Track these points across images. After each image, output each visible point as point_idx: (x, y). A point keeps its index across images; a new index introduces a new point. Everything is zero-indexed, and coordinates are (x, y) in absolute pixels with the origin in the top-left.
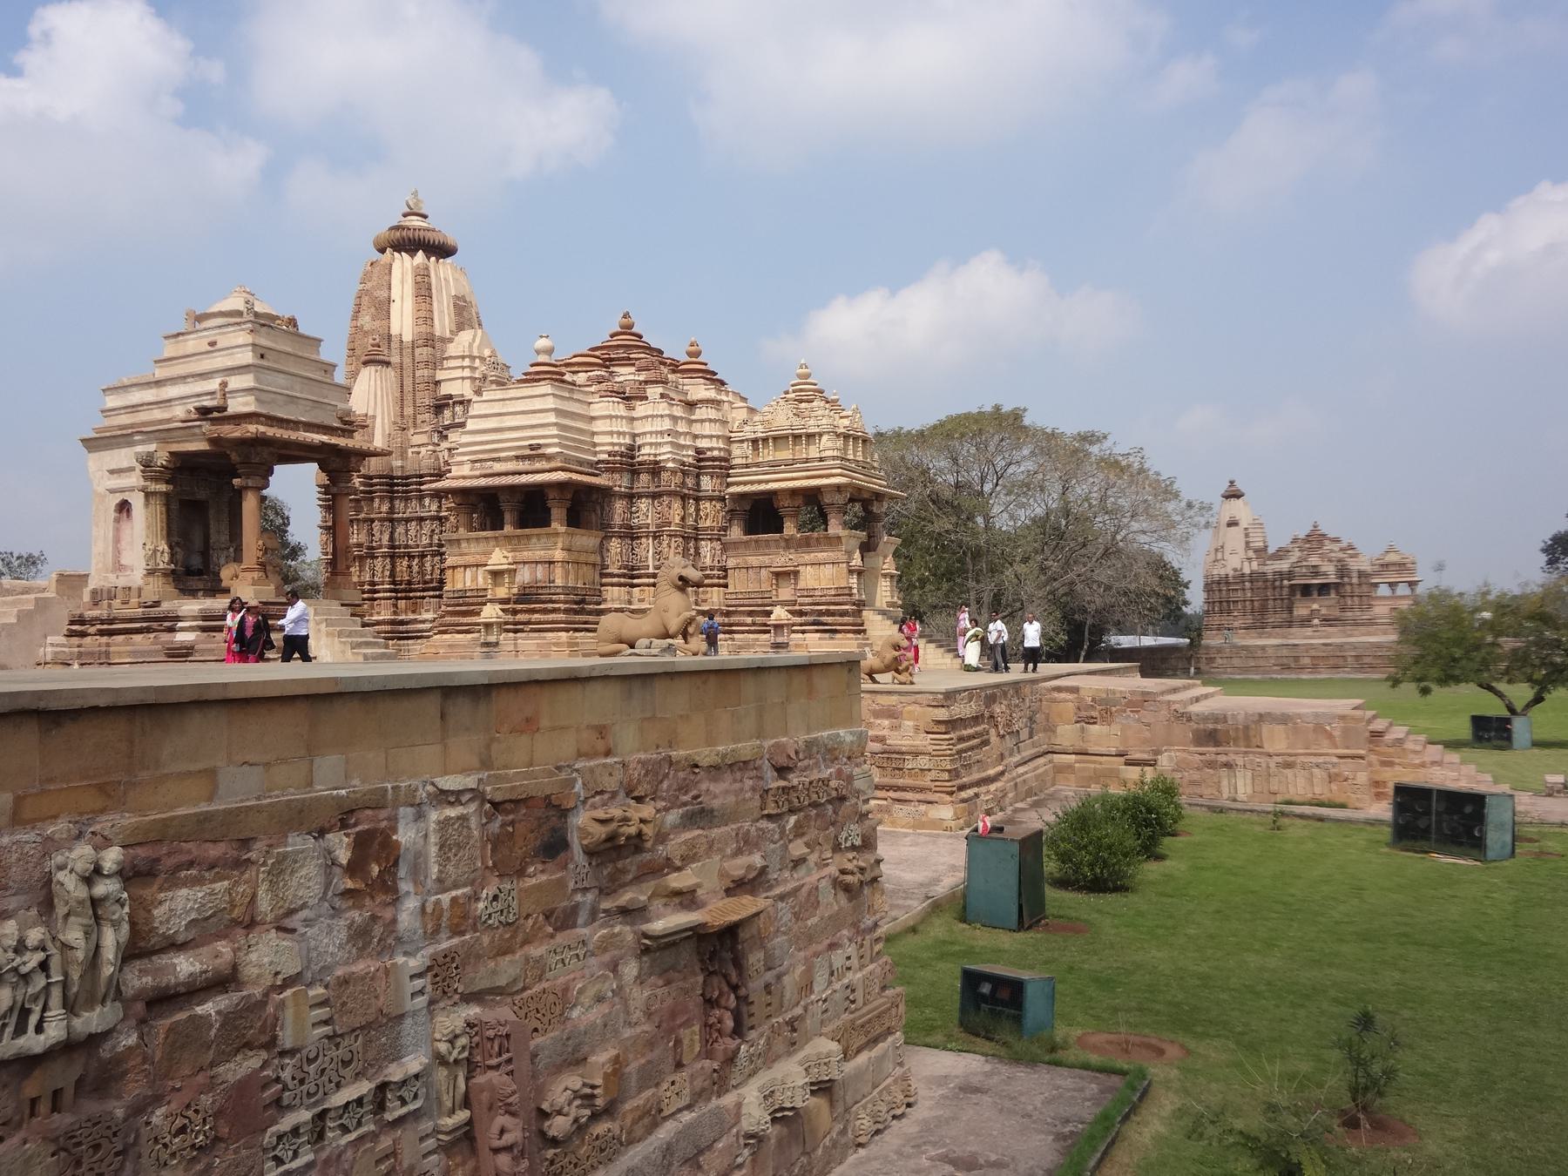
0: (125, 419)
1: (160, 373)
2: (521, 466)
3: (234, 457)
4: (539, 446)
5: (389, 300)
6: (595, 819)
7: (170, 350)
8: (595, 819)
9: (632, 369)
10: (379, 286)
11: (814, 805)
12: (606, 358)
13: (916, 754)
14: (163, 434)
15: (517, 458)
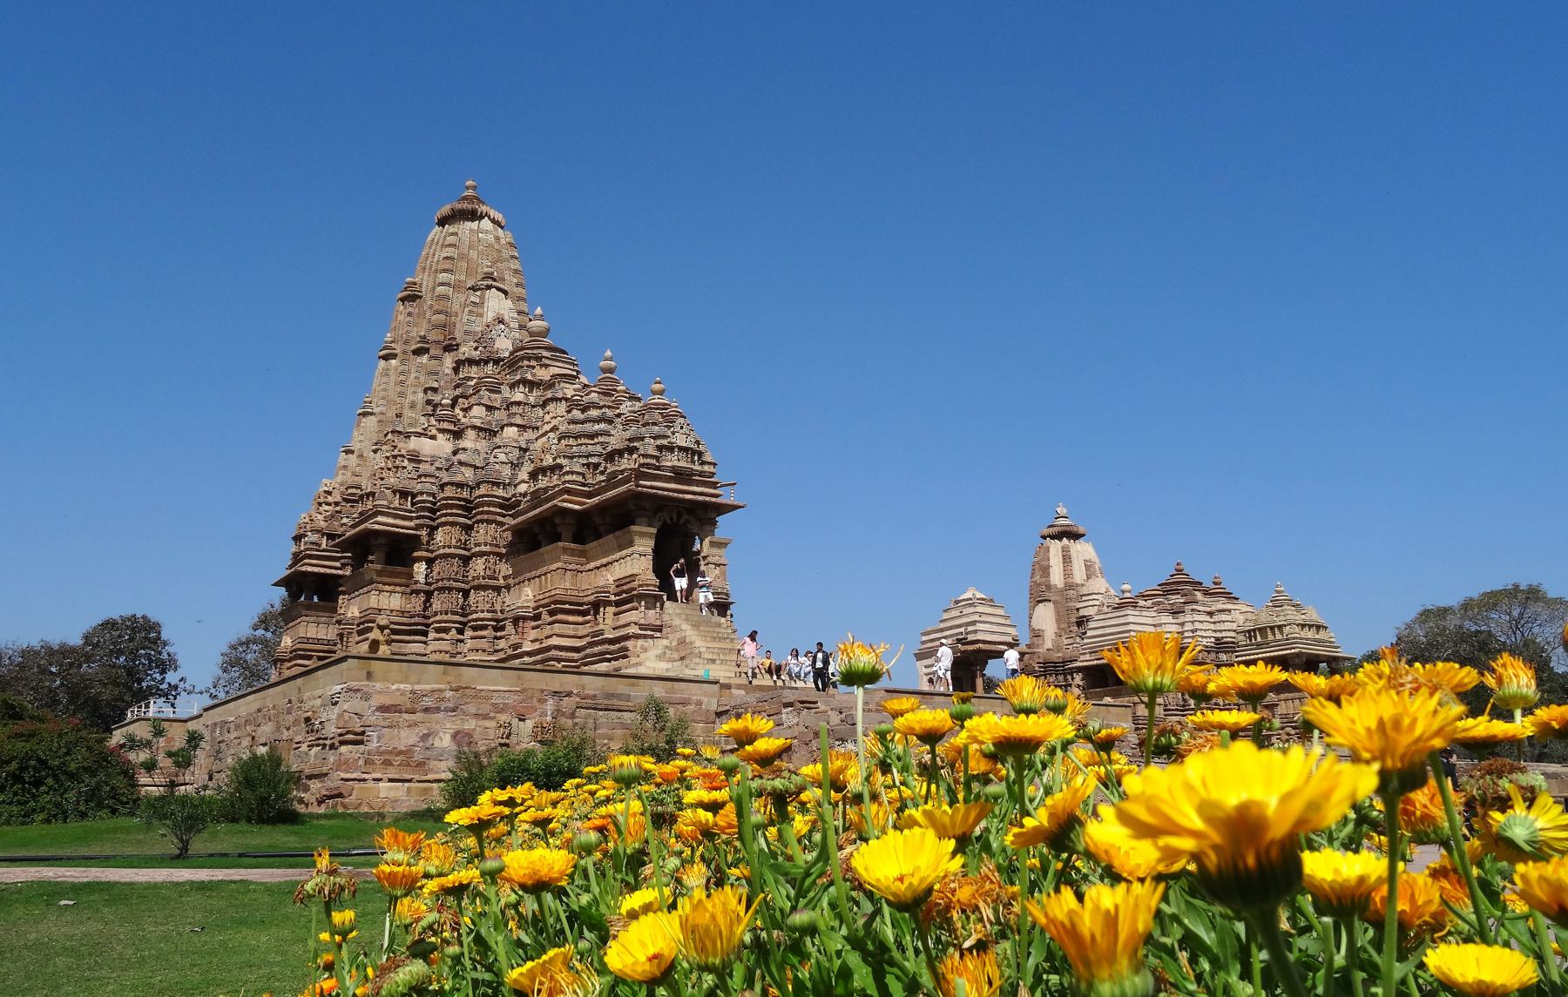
1: (943, 625)
3: (972, 658)
5: (1049, 567)
6: (741, 507)
7: (945, 616)
8: (741, 507)
9: (1179, 596)
10: (1043, 560)
11: (389, 469)
12: (1168, 588)
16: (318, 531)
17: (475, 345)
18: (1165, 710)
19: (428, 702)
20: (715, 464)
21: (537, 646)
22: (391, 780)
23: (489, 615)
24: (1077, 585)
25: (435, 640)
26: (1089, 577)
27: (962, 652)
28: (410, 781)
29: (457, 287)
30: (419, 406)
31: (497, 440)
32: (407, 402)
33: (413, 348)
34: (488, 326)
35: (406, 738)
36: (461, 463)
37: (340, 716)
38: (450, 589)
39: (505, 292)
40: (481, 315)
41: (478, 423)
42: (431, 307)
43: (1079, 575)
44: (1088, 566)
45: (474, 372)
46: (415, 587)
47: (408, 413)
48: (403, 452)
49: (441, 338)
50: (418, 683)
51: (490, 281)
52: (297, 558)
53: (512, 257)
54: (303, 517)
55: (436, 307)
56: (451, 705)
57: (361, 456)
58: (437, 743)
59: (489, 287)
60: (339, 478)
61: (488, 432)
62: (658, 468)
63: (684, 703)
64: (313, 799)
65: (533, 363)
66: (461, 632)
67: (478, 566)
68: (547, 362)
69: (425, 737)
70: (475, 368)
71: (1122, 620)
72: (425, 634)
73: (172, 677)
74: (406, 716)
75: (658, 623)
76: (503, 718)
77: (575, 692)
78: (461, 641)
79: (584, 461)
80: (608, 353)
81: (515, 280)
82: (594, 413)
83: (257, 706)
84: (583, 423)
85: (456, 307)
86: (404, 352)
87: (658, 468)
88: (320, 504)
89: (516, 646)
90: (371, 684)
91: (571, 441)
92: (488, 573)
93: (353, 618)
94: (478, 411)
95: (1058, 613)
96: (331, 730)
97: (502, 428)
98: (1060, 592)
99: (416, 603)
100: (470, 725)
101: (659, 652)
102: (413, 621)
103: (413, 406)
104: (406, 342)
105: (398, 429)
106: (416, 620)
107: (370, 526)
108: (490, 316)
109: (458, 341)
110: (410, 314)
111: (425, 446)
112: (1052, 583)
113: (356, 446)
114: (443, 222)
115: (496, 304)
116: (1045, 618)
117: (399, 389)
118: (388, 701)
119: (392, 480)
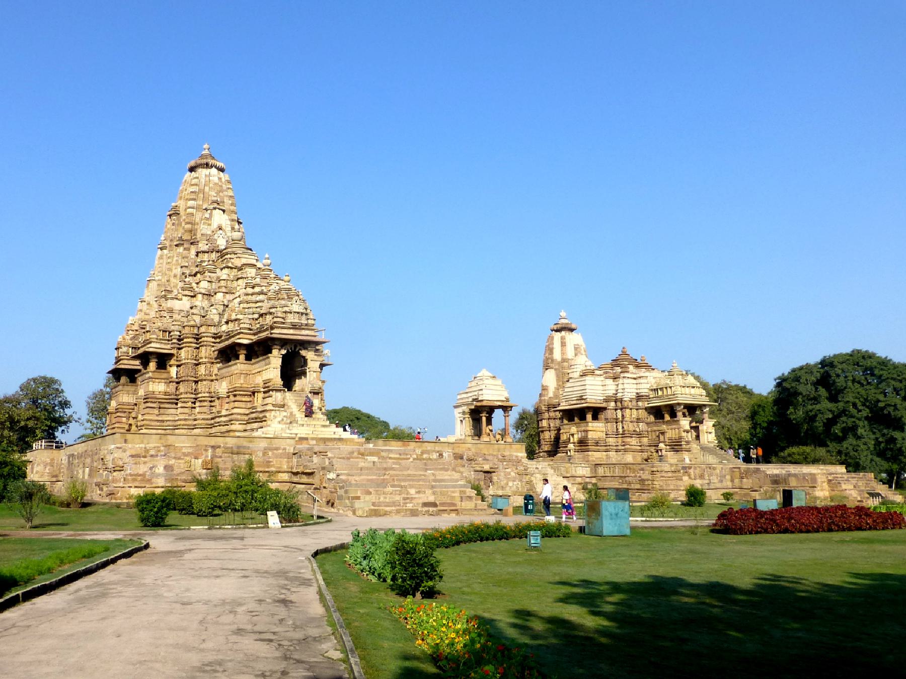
0: (461, 401)
1: (467, 391)
2: (578, 402)
4: (582, 396)
12: (616, 363)
13: (648, 480)
14: (468, 405)
15: (577, 400)
16: (127, 346)
17: (206, 242)
18: (606, 435)
19: (152, 452)
20: (314, 320)
21: (228, 413)
22: (136, 487)
23: (207, 395)
24: (569, 359)
25: (182, 407)
26: (576, 355)
27: (476, 406)
28: (145, 487)
29: (198, 208)
30: (178, 276)
31: (212, 299)
32: (172, 274)
33: (175, 243)
34: (213, 232)
35: (142, 469)
36: (193, 314)
37: (113, 459)
38: (188, 381)
39: (224, 211)
40: (209, 225)
41: (203, 291)
42: (184, 220)
43: (570, 353)
44: (577, 348)
45: (206, 257)
46: (171, 380)
47: (173, 280)
48: (165, 309)
49: (189, 238)
50: (148, 444)
51: (218, 205)
52: (118, 360)
53: (229, 188)
54: (120, 339)
55: (187, 221)
56: (163, 453)
57: (149, 304)
58: (157, 471)
59: (215, 208)
60: (138, 317)
61: (209, 295)
62: (284, 323)
63: (277, 449)
64: (104, 495)
65: (233, 256)
66: (194, 403)
67: (202, 370)
68: (240, 255)
69: (151, 468)
70: (206, 255)
71: (582, 383)
72: (177, 404)
73: (68, 412)
74: (142, 459)
75: (282, 403)
76: (188, 458)
77: (222, 446)
78: (195, 408)
79: (251, 316)
80: (267, 256)
81: (230, 202)
82: (257, 289)
83: (85, 448)
84: (252, 295)
85: (197, 220)
86: (170, 246)
87: (284, 323)
88: (128, 331)
89: (219, 412)
90: (126, 445)
91: (245, 305)
92: (207, 372)
93: (141, 396)
94: (204, 284)
95: (557, 376)
96: (110, 466)
97: (215, 294)
98: (559, 363)
99: (172, 388)
100: (172, 462)
101: (280, 419)
102: (170, 397)
103: (175, 276)
104: (171, 240)
105: (167, 289)
106: (173, 397)
107: (147, 350)
108: (215, 226)
109: (198, 239)
110: (173, 224)
111: (176, 305)
112: (554, 358)
113: (147, 299)
114: (192, 169)
115: (219, 218)
116: (550, 379)
117: (168, 266)
118: (134, 453)
119: (159, 324)
